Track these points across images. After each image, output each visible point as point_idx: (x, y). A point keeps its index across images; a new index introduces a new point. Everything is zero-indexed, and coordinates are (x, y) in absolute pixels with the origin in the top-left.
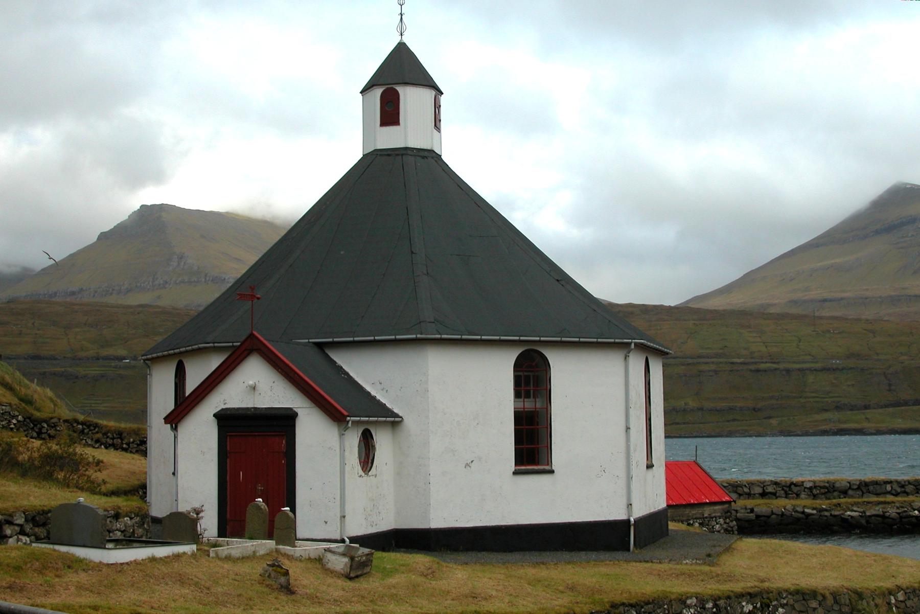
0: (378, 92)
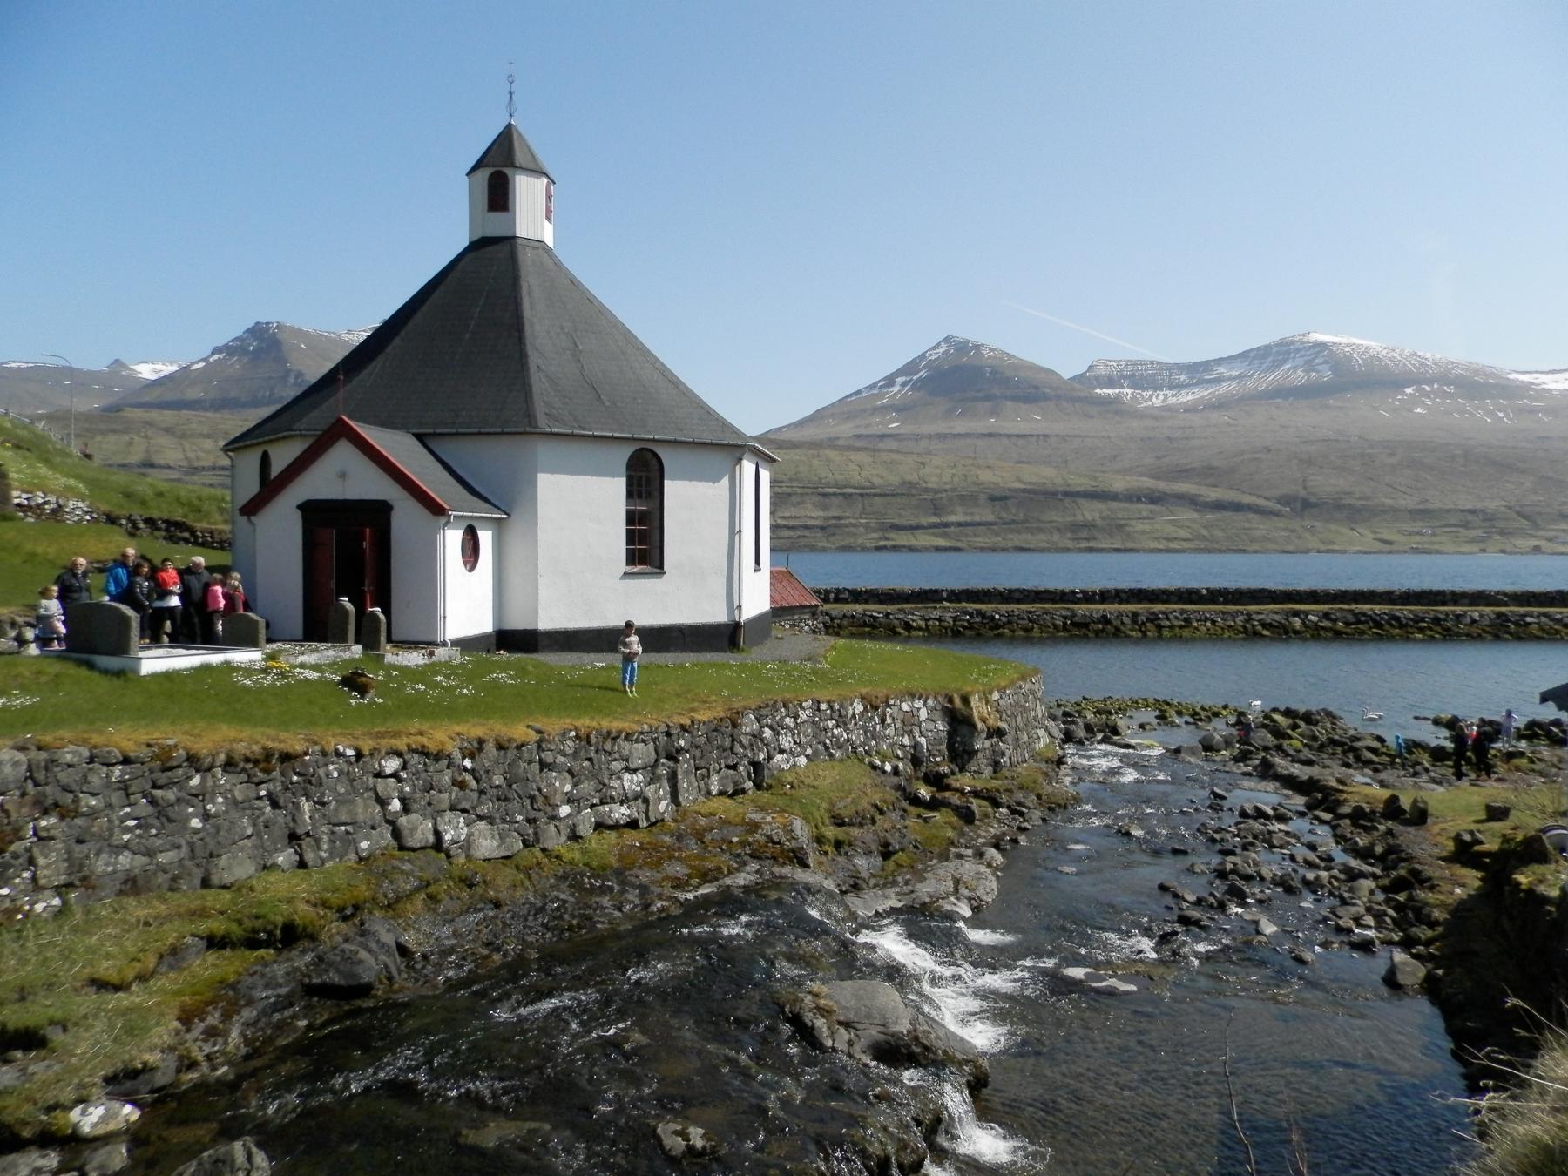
0: (484, 174)
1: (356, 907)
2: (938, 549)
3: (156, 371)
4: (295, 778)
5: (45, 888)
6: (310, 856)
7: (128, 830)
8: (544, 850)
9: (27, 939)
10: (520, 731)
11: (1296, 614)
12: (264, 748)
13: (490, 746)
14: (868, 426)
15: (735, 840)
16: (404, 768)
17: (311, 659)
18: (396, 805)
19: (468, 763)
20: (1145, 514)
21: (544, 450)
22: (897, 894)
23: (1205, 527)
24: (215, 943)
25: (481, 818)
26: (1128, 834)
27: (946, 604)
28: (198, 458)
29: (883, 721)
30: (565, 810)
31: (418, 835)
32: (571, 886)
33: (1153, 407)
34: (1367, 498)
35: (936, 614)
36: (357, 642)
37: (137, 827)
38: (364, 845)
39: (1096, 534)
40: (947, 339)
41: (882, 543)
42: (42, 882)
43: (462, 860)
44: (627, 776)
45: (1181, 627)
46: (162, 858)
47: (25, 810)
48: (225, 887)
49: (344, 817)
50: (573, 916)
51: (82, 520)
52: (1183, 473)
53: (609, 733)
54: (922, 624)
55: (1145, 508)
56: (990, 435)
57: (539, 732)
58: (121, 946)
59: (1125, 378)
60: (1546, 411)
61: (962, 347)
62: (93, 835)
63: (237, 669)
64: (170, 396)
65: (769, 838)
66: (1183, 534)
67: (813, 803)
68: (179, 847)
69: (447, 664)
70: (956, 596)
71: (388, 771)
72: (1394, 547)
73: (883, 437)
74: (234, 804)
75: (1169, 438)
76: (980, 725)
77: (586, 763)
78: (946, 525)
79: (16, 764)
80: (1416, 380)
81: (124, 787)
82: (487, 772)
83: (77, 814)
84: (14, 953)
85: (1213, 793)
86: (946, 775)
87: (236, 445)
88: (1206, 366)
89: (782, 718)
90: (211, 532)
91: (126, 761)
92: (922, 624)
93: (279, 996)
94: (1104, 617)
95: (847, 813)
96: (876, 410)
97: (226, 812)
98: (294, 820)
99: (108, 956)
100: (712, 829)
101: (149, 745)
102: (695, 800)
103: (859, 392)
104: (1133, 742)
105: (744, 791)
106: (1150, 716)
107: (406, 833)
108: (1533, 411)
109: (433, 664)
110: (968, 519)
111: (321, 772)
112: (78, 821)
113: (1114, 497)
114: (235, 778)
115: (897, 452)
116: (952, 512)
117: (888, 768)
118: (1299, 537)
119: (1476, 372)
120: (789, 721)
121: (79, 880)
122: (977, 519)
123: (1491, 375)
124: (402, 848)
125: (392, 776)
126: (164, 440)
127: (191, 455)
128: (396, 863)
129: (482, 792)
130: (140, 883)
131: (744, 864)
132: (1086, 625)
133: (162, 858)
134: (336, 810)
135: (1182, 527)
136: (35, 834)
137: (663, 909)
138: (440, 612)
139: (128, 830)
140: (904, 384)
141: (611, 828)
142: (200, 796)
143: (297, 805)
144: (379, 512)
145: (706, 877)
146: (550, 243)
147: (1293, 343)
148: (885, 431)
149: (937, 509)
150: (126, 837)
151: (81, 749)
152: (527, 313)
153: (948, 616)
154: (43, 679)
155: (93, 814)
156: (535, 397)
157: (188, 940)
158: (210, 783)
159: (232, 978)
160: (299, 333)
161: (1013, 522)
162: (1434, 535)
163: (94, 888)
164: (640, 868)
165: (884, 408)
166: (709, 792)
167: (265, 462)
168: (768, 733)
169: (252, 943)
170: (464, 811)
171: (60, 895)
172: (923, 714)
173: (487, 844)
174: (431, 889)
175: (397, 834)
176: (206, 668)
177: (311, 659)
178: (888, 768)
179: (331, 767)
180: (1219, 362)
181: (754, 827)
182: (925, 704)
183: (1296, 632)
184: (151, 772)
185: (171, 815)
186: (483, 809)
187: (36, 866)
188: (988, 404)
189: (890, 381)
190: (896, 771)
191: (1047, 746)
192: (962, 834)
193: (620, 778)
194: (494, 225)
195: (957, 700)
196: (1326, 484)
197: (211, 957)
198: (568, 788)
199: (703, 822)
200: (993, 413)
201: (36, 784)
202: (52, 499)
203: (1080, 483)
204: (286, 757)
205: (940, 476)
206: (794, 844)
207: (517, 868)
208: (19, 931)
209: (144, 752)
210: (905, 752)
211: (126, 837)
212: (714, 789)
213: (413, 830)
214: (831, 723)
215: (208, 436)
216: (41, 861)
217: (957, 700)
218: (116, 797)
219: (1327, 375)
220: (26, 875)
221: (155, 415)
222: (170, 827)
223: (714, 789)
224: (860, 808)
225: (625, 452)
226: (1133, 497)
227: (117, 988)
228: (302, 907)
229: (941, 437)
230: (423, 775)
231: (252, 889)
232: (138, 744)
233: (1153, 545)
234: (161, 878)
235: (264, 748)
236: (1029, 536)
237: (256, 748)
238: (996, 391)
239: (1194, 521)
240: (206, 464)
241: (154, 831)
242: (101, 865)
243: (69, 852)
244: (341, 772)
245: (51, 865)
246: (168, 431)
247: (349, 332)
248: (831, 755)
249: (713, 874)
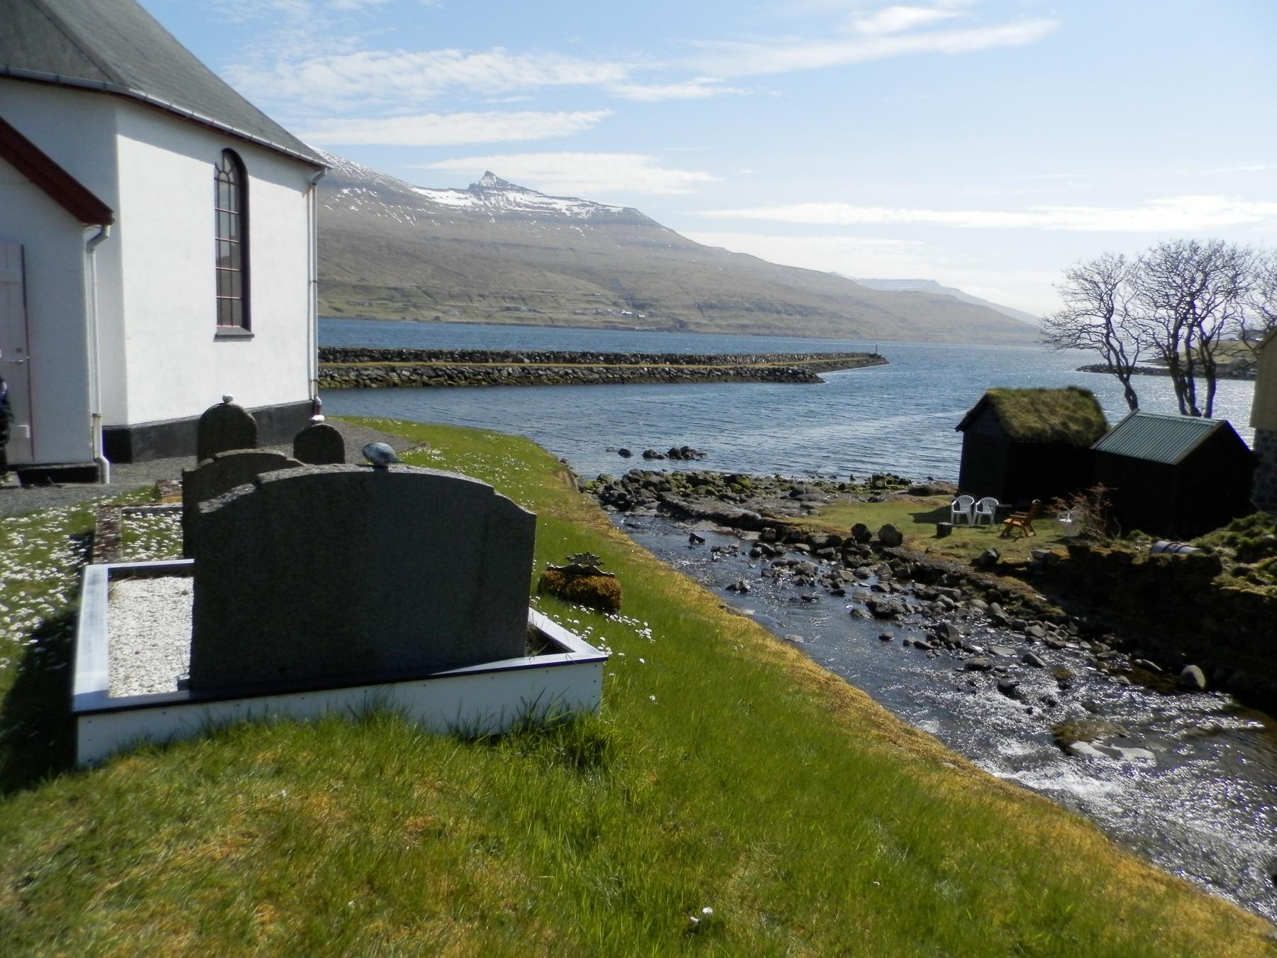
11: (393, 370)
21: (123, 116)
60: (436, 218)
72: (344, 314)
80: (351, 185)
108: (428, 217)
119: (391, 183)
123: (399, 186)
162: (370, 305)
183: (395, 385)
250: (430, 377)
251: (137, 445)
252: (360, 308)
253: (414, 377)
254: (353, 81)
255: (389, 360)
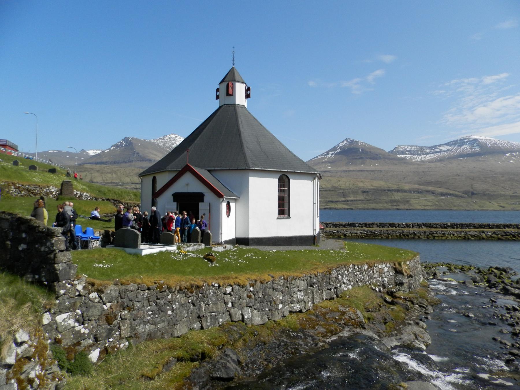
1: (223, 345)
2: (345, 209)
3: (94, 153)
4: (200, 295)
5: (123, 338)
6: (204, 325)
7: (149, 315)
8: (274, 321)
9: (119, 359)
10: (266, 277)
11: (483, 232)
12: (191, 284)
13: (258, 282)
14: (320, 168)
15: (337, 318)
16: (232, 291)
17: (190, 249)
18: (230, 305)
19: (251, 289)
20: (416, 197)
21: (251, 173)
22: (396, 339)
23: (437, 202)
24: (179, 359)
25: (255, 309)
26: (468, 316)
27: (358, 228)
28: (106, 180)
29: (373, 272)
30: (280, 306)
31: (237, 316)
32: (286, 335)
33: (417, 161)
34: (495, 192)
35: (354, 231)
36: (202, 242)
37: (152, 314)
38: (221, 320)
39: (399, 204)
40: (346, 139)
41: (326, 207)
42: (123, 336)
43: (250, 326)
44: (298, 293)
45: (442, 237)
46: (160, 326)
47: (118, 308)
48: (178, 337)
49: (215, 310)
50: (292, 349)
51: (87, 199)
52: (429, 183)
53: (293, 277)
54: (350, 235)
55: (416, 195)
56: (361, 171)
57: (273, 277)
58: (149, 361)
59: (408, 151)
61: (352, 142)
62: (138, 317)
63: (171, 253)
64: (98, 161)
65: (350, 317)
66: (430, 204)
67: (359, 304)
68: (164, 322)
69: (230, 250)
70: (361, 225)
71: (228, 292)
72: (505, 209)
73: (325, 171)
74: (181, 305)
75: (423, 172)
76: (405, 274)
77: (286, 288)
78: (348, 201)
79: (115, 291)
80: (511, 151)
81: (148, 299)
82: (257, 292)
83: (134, 310)
84: (115, 364)
85: (491, 300)
86: (394, 292)
87: (142, 175)
88: (435, 147)
89: (344, 271)
90: (127, 204)
91: (149, 289)
92: (350, 235)
93: (203, 382)
94: (414, 233)
95: (370, 307)
96: (323, 163)
97: (179, 308)
98: (199, 311)
99: (146, 365)
100: (328, 313)
101: (155, 283)
102: (319, 302)
103: (317, 157)
104: (446, 279)
105: (333, 298)
106: (445, 269)
107: (233, 315)
109: (226, 251)
110: (355, 199)
111: (208, 292)
112: (134, 312)
113: (405, 191)
114: (181, 295)
115: (331, 176)
116: (349, 197)
117: (377, 289)
118: (471, 205)
120: (346, 272)
121: (134, 335)
122: (358, 199)
124: (232, 321)
125: (229, 294)
126: (96, 174)
127: (104, 179)
128: (231, 327)
129: (255, 300)
130: (152, 336)
131: (344, 328)
132: (408, 236)
133: (160, 326)
134: (212, 307)
135: (429, 201)
136: (121, 317)
137: (323, 346)
138: (220, 232)
139: (149, 315)
140: (332, 154)
141: (294, 312)
142: (171, 303)
143: (200, 306)
144: (200, 197)
145: (333, 333)
146: (246, 106)
147: (465, 139)
148: (326, 170)
149: (344, 196)
150: (148, 318)
151: (135, 284)
152: (241, 129)
153: (359, 232)
154: (111, 257)
155: (139, 310)
156: (247, 157)
157: (171, 358)
158: (174, 297)
159: (188, 375)
160: (138, 140)
161: (370, 200)
163: (138, 338)
164: (308, 329)
165: (326, 162)
166: (323, 299)
167: (154, 180)
168: (340, 277)
169: (192, 360)
170: (250, 307)
171: (128, 341)
172: (386, 270)
173: (258, 320)
174: (243, 338)
175: (230, 315)
176: (161, 252)
177: (190, 249)
178: (377, 289)
179: (211, 291)
180: (440, 146)
181: (343, 313)
182: (386, 266)
183: (483, 239)
184: (157, 293)
185: (162, 309)
186: (256, 306)
187: (120, 330)
188: (360, 160)
189: (328, 153)
190: (380, 291)
191: (423, 281)
192: (406, 315)
193: (296, 294)
194: (228, 101)
195: (397, 265)
196: (479, 187)
197: (179, 366)
198: (281, 298)
199: (324, 310)
200: (362, 163)
201: (122, 298)
202: (79, 192)
203: (394, 187)
204: (198, 287)
205: (345, 184)
206: (359, 320)
207: (267, 328)
208: (116, 355)
209: (154, 286)
210: (380, 283)
211: (148, 318)
212: (325, 298)
213: (235, 314)
214: (358, 273)
215: (110, 173)
216: (122, 328)
217: (397, 265)
218: (146, 303)
219: (478, 149)
220: (118, 333)
221: (94, 166)
222: (162, 314)
223: (325, 298)
224: (374, 305)
225: (279, 175)
226: (410, 191)
227: (151, 379)
228: (206, 345)
229: (345, 171)
230: (238, 293)
231: (187, 338)
232: (152, 283)
233: (419, 207)
234: (159, 333)
235: (191, 284)
236: (376, 205)
237: (188, 284)
238: (363, 156)
239: (433, 199)
240: (109, 181)
241: (157, 316)
242: (141, 329)
243: (131, 324)
244: (213, 292)
245: (125, 330)
246: (98, 171)
247: (154, 140)
248: (358, 285)
249: (335, 332)
250: (502, 236)
251: (251, 242)
252: (514, 206)
253: (494, 236)
254: (498, 110)
255: (483, 228)
